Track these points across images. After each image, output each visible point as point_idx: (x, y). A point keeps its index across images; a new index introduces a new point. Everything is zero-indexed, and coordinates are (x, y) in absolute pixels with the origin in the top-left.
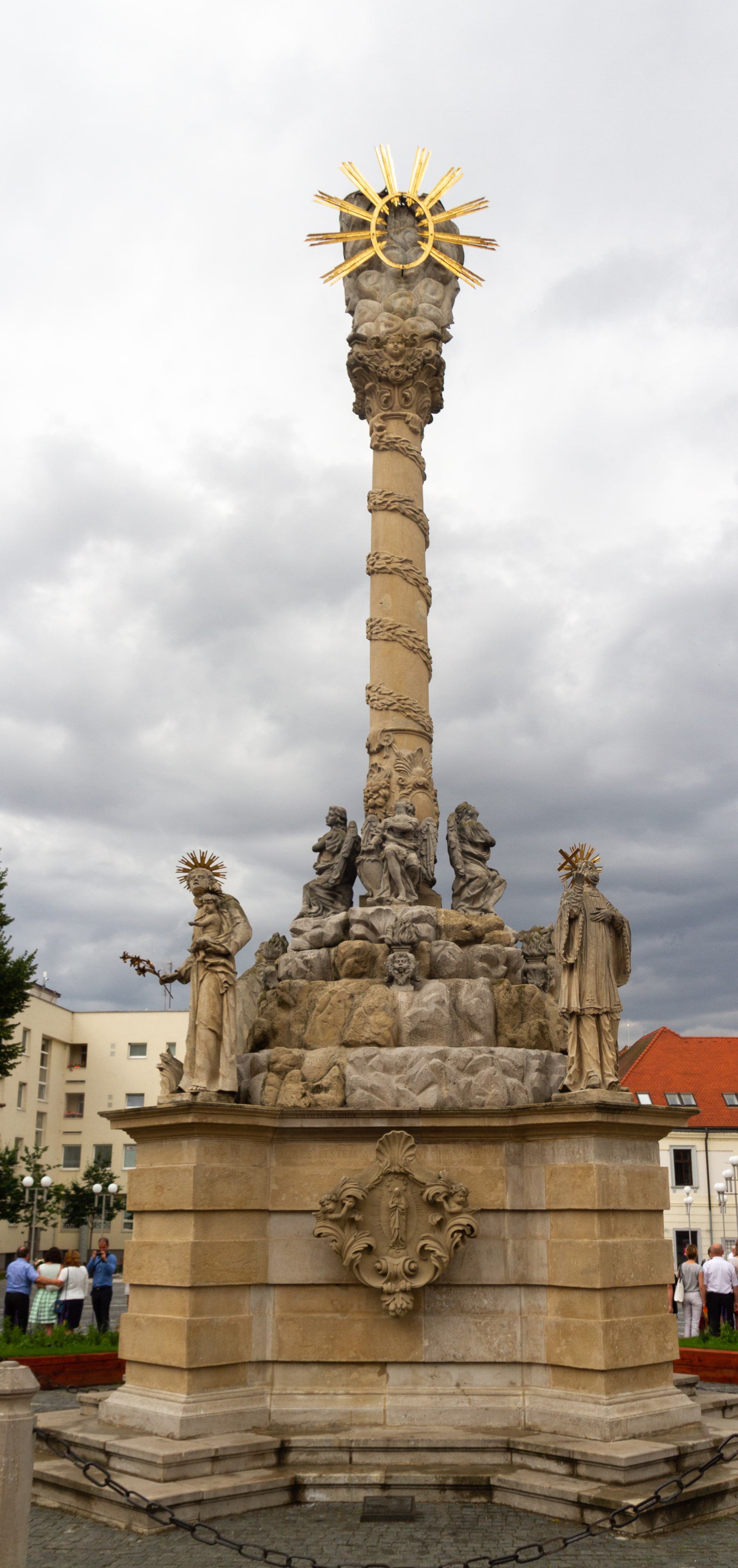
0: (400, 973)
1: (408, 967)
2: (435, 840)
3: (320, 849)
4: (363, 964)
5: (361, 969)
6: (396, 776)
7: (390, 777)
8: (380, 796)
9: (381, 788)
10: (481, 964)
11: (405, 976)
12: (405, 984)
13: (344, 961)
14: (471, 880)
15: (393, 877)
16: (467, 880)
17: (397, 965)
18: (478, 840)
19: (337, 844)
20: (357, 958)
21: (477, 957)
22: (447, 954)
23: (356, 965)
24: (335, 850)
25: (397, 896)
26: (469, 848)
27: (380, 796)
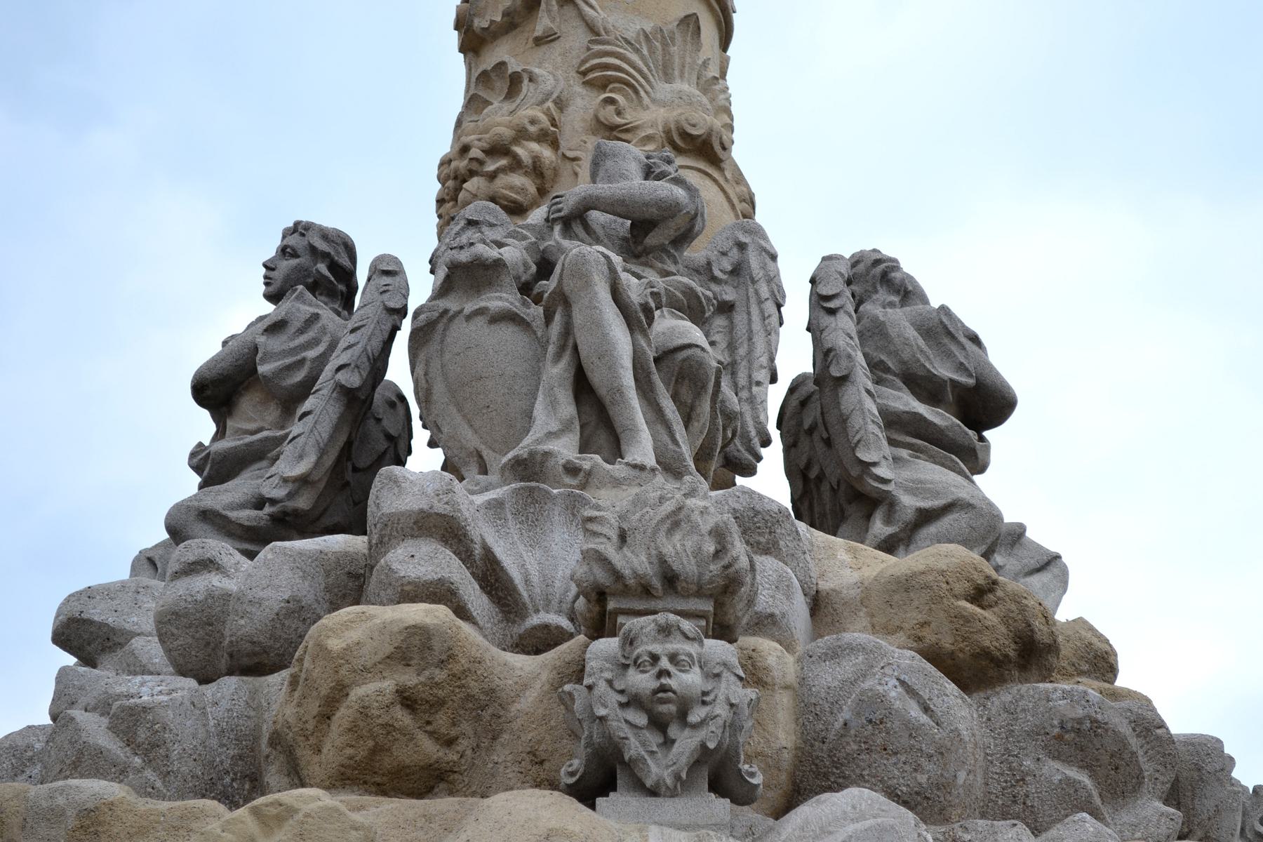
0: (659, 724)
1: (704, 699)
2: (770, 307)
3: (217, 390)
4: (441, 721)
5: (430, 749)
6: (584, 104)
7: (561, 104)
8: (516, 165)
9: (521, 135)
10: (1056, 771)
11: (686, 743)
12: (682, 786)
13: (340, 692)
14: (926, 517)
15: (597, 377)
16: (909, 515)
17: (642, 681)
18: (944, 371)
19: (312, 354)
20: (409, 678)
21: (1032, 734)
22: (894, 693)
23: (402, 717)
24: (299, 376)
25: (615, 450)
26: (906, 402)
27: (516, 165)
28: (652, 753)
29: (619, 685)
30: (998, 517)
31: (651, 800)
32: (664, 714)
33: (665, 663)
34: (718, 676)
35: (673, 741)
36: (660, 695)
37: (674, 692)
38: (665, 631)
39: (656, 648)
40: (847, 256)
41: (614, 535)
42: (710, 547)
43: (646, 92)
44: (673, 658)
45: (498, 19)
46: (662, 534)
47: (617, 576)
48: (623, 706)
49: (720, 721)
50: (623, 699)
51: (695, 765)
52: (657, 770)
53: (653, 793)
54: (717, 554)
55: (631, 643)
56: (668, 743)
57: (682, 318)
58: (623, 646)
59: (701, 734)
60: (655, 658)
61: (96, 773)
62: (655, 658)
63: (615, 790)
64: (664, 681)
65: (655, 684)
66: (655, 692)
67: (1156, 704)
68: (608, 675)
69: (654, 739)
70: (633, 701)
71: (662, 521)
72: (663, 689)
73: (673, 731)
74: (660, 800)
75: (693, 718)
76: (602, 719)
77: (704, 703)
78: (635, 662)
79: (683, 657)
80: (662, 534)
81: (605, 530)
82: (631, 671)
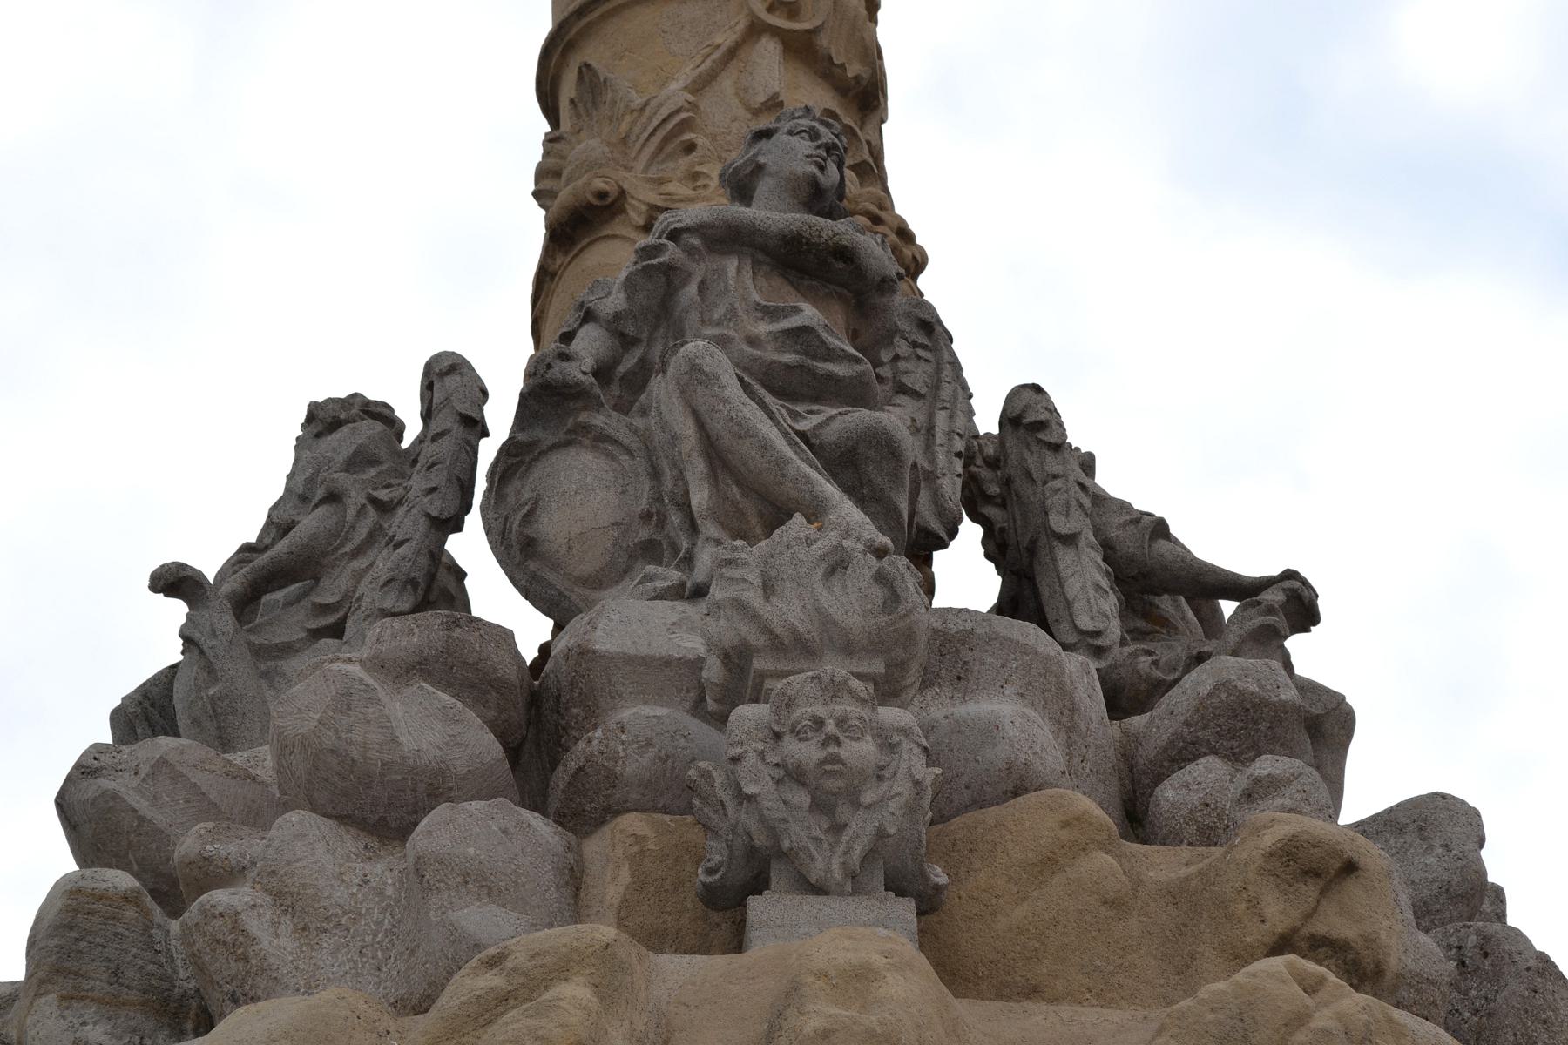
0: (822, 805)
11: (861, 829)
12: (856, 884)
17: (807, 752)
28: (817, 840)
29: (773, 758)
30: (1485, 874)
32: (830, 795)
33: (831, 727)
36: (829, 767)
38: (835, 689)
39: (821, 711)
44: (841, 722)
45: (850, 74)
47: (767, 630)
51: (869, 857)
52: (827, 864)
53: (819, 890)
55: (788, 705)
56: (838, 829)
57: (817, 469)
58: (777, 712)
60: (819, 723)
61: (327, 627)
62: (819, 723)
63: (768, 888)
64: (832, 749)
65: (819, 755)
66: (824, 762)
68: (760, 746)
69: (819, 826)
70: (794, 775)
72: (834, 759)
73: (843, 812)
75: (868, 797)
78: (793, 730)
79: (852, 722)
82: (787, 738)
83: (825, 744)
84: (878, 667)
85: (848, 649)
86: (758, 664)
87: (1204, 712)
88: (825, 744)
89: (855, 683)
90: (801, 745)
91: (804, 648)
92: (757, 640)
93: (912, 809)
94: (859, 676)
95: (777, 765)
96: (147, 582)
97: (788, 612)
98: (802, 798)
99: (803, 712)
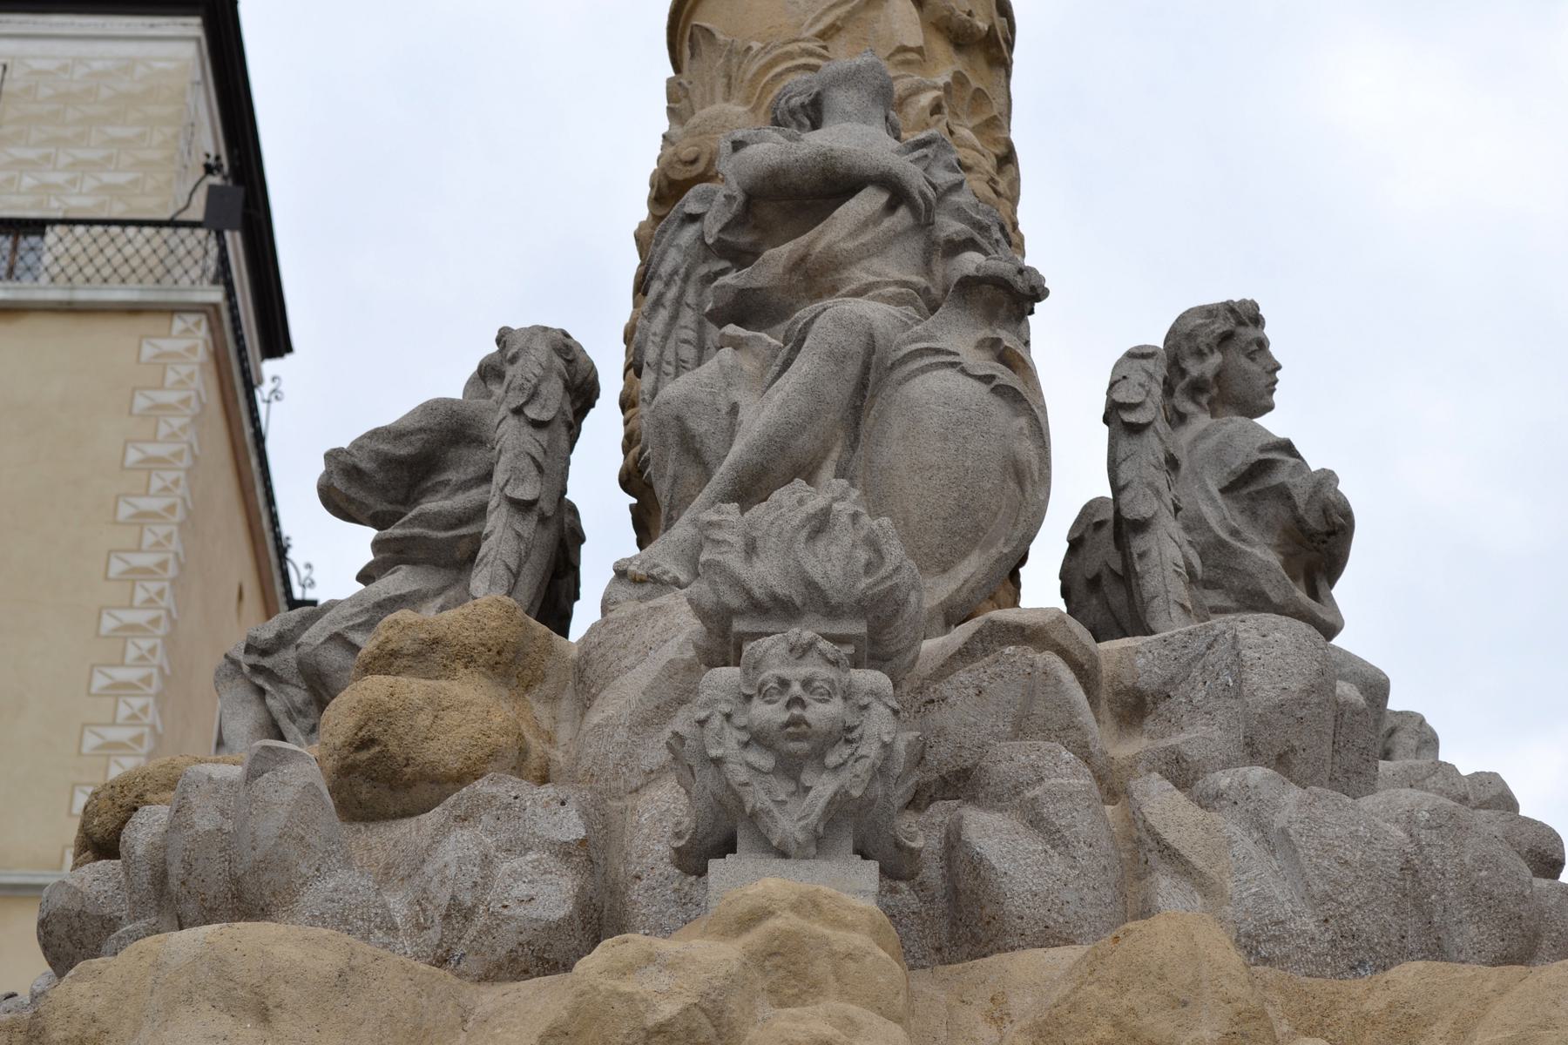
12: (820, 842)
17: (768, 713)
29: (740, 720)
31: (778, 863)
33: (796, 689)
34: (865, 707)
35: (807, 789)
36: (791, 729)
37: (809, 726)
38: (801, 651)
39: (786, 672)
40: (1028, 262)
41: (737, 541)
42: (863, 555)
43: (890, 577)
46: (800, 546)
48: (746, 745)
49: (868, 762)
50: (745, 737)
52: (788, 825)
53: (783, 854)
54: (869, 568)
59: (845, 776)
62: (784, 684)
63: (734, 851)
64: (796, 711)
66: (787, 725)
67: (1429, 721)
69: (783, 788)
70: (757, 738)
71: (797, 529)
74: (791, 861)
76: (718, 762)
77: (848, 742)
79: (817, 684)
80: (800, 546)
81: (732, 539)
82: (756, 701)
83: (788, 706)
84: (859, 628)
85: (833, 611)
86: (739, 626)
87: (415, 518)
88: (788, 706)
89: (824, 645)
90: (770, 707)
91: (778, 609)
92: (734, 600)
93: (880, 772)
94: (826, 637)
95: (744, 728)
96: (288, 358)
97: (765, 574)
98: (765, 761)
99: (769, 674)
